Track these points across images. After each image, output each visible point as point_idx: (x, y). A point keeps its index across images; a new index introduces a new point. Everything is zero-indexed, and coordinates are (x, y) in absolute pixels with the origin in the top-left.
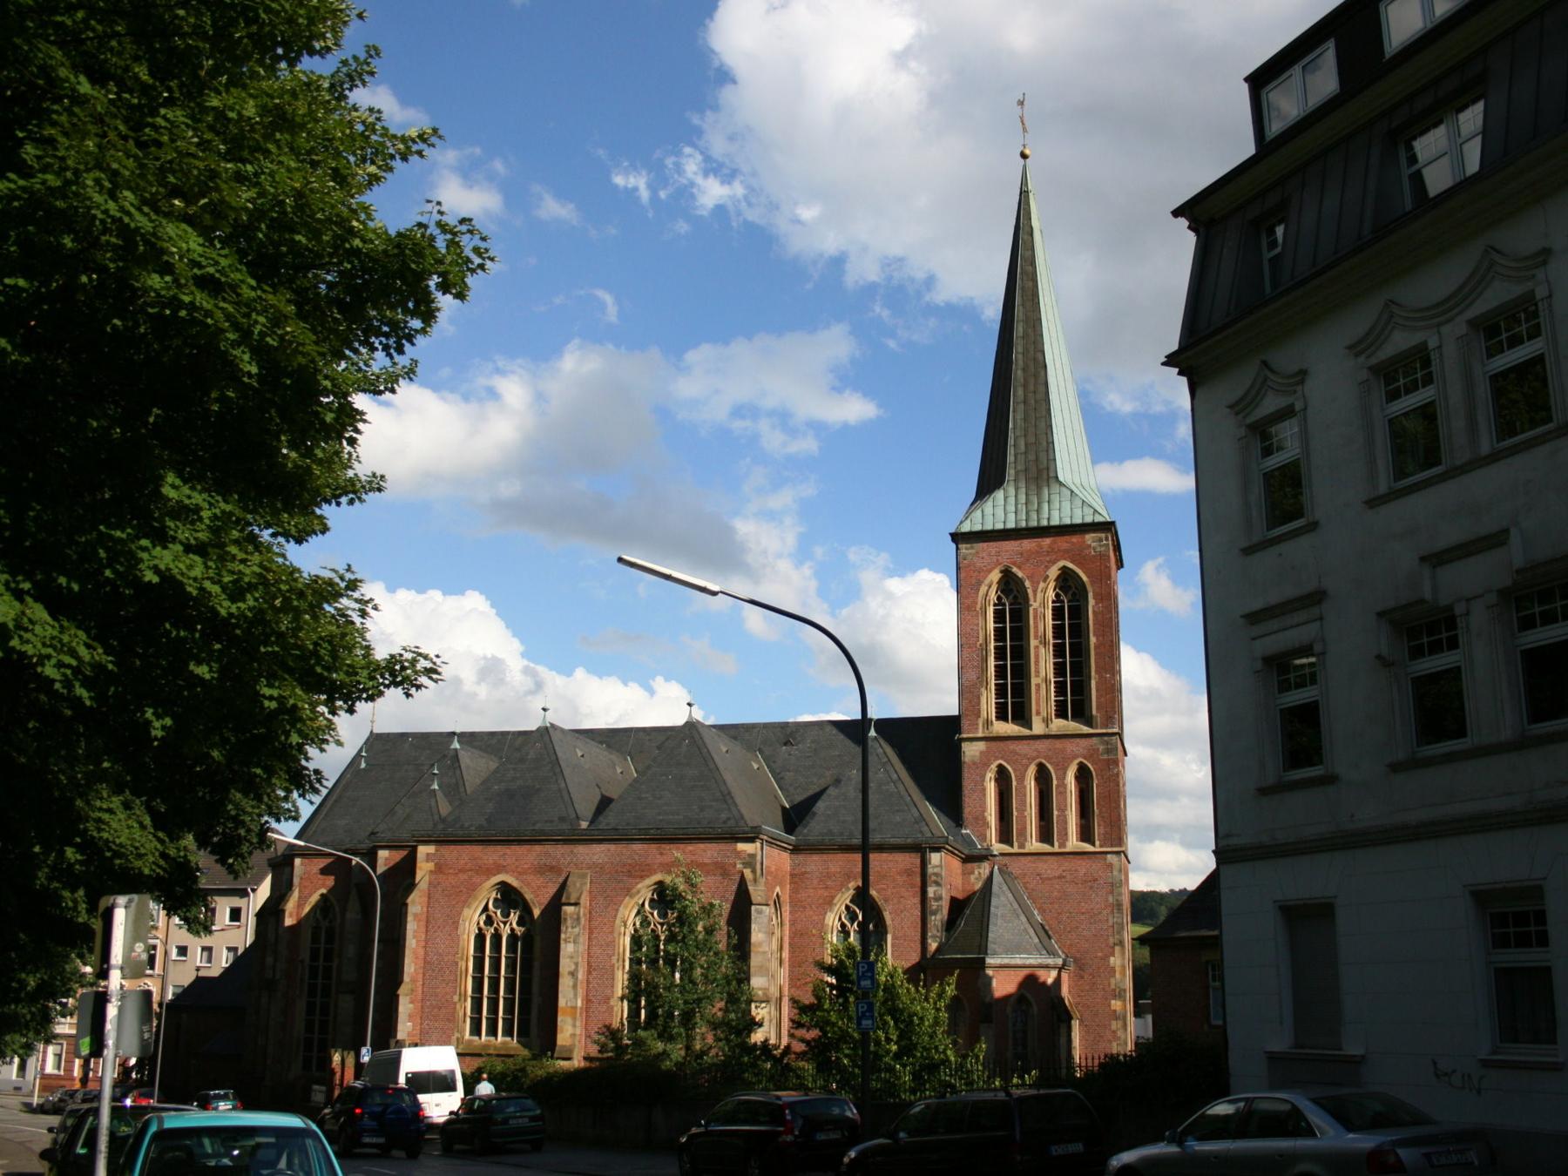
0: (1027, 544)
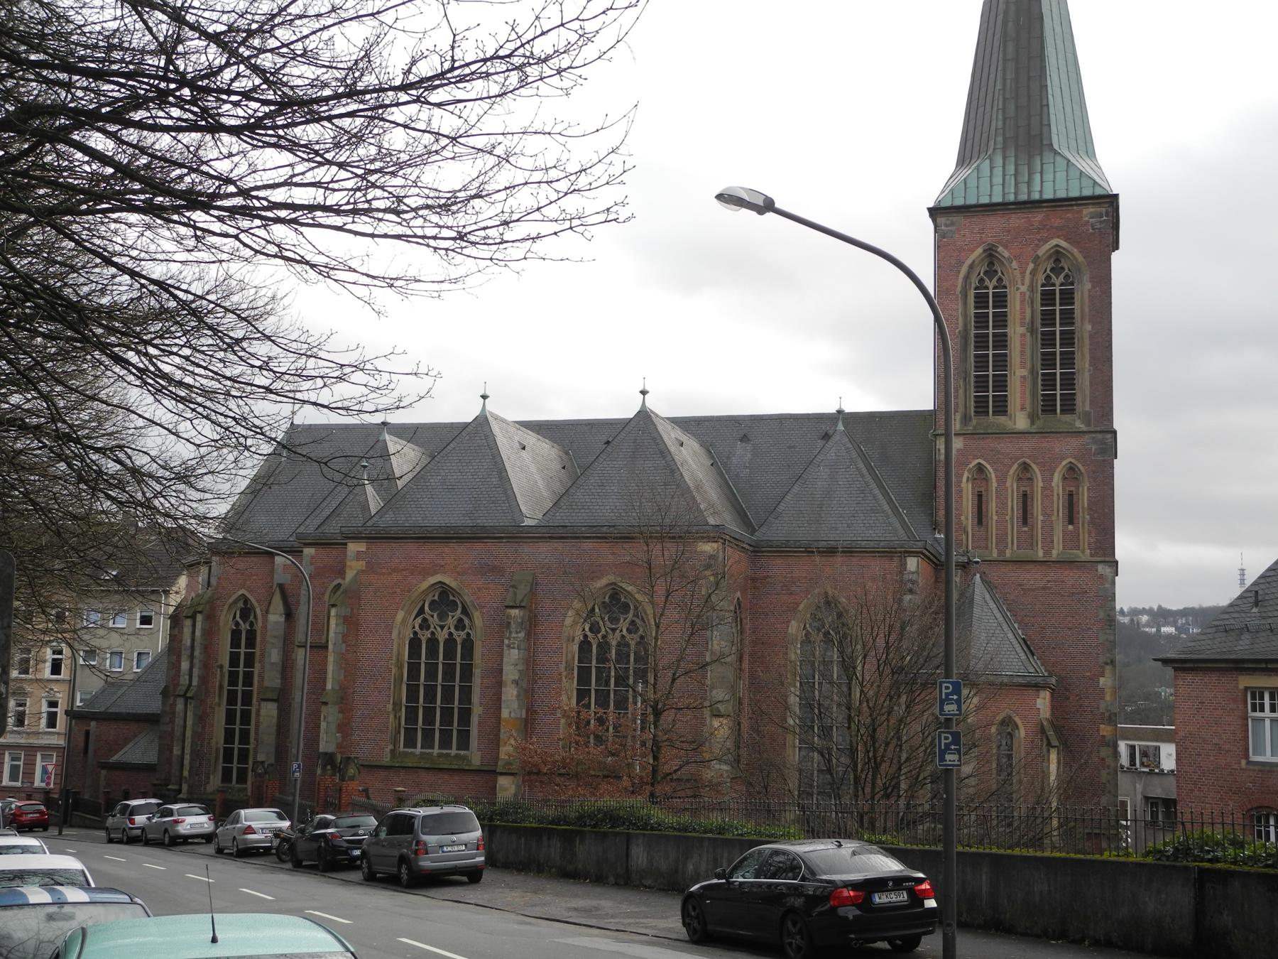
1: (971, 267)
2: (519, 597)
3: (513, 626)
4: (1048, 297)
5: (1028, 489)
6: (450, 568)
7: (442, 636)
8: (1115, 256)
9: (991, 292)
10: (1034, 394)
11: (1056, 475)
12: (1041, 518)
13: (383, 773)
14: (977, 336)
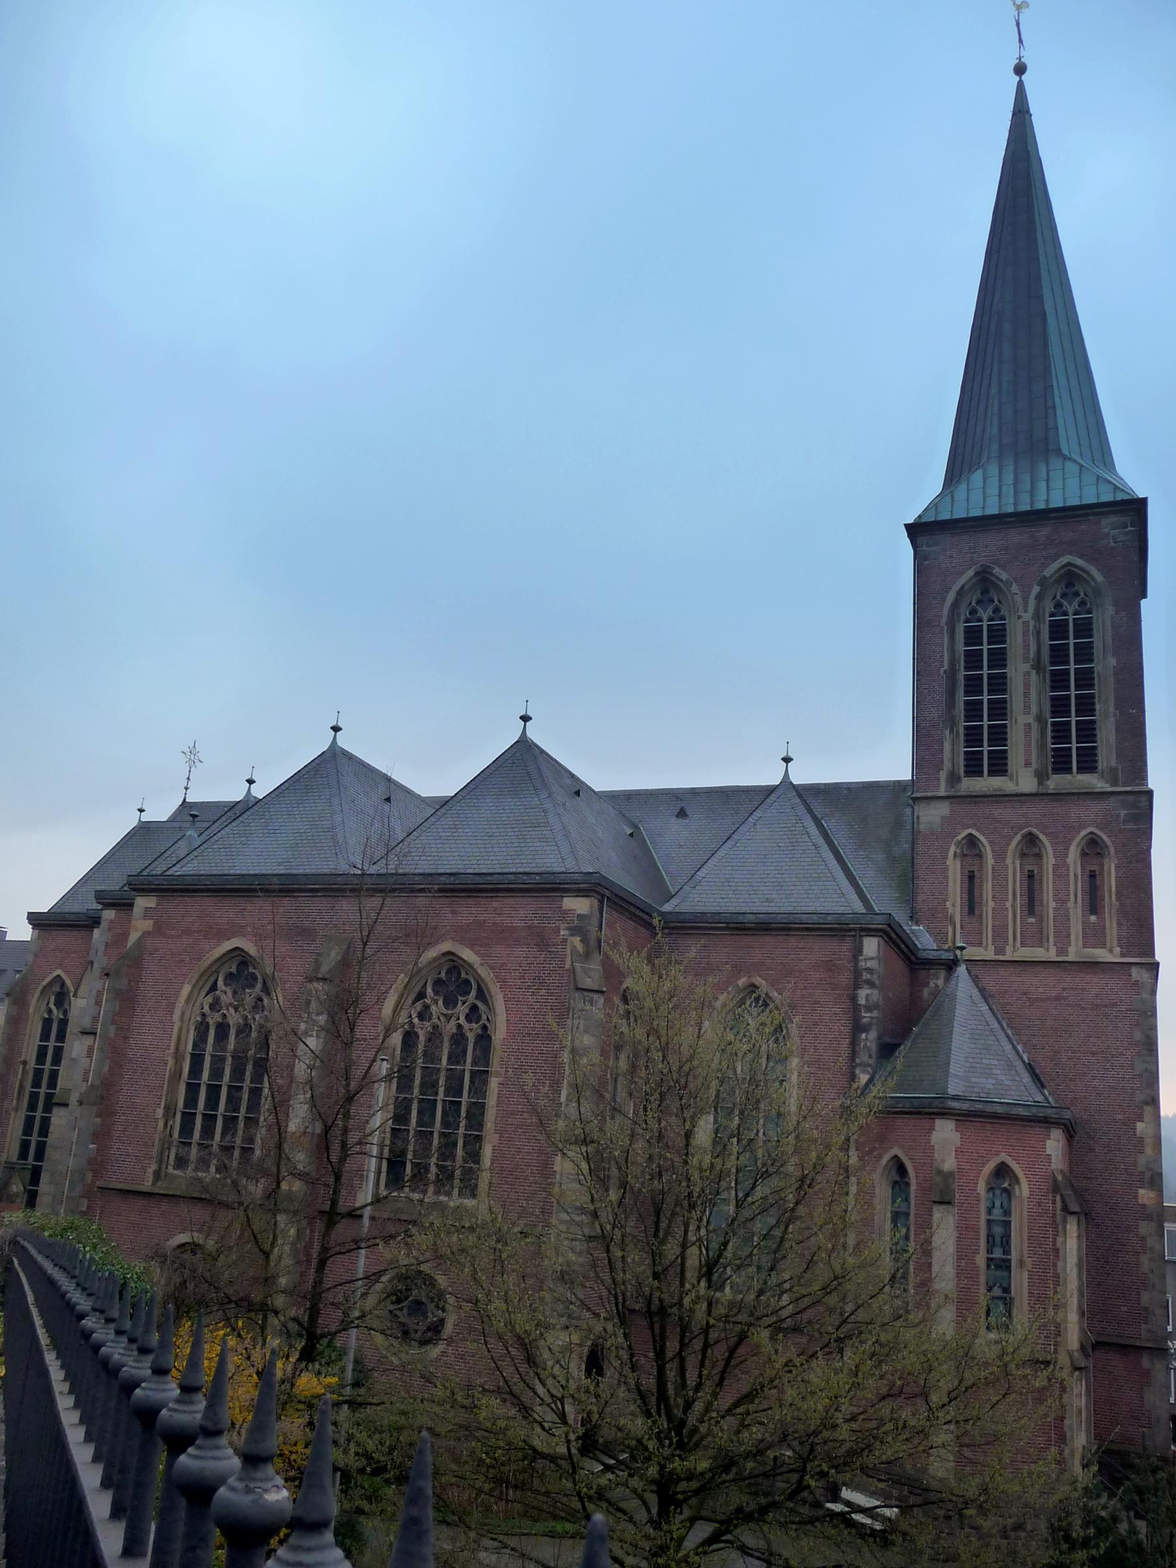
0: (1016, 537)
1: (961, 593)
2: (324, 969)
3: (314, 1006)
4: (1058, 629)
5: (1035, 868)
6: (245, 931)
7: (234, 1018)
8: (1143, 603)
9: (985, 624)
10: (1042, 746)
11: (1073, 848)
12: (1052, 905)
13: (141, 1202)
14: (967, 678)
